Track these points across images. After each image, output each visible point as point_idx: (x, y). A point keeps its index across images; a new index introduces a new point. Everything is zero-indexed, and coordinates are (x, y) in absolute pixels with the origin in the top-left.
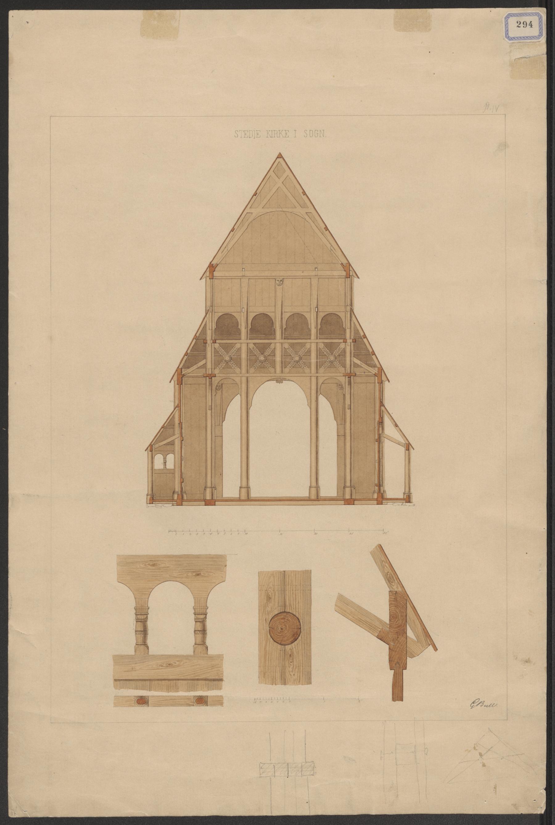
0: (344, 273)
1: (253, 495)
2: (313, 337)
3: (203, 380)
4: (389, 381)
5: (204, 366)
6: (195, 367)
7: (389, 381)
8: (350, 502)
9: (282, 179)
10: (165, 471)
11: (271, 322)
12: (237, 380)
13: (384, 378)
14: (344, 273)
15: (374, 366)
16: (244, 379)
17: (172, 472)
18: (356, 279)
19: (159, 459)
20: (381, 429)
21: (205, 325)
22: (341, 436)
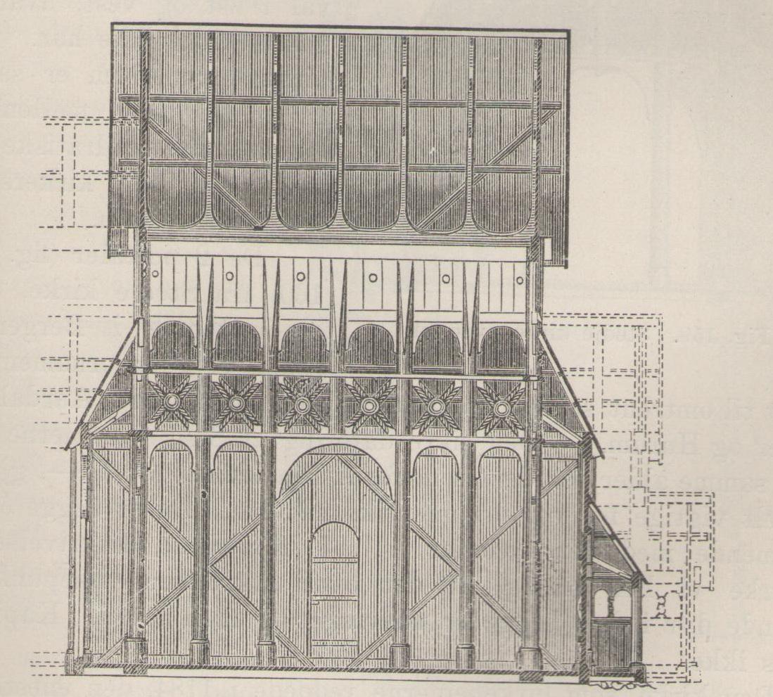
13: (595, 452)
18: (599, 460)
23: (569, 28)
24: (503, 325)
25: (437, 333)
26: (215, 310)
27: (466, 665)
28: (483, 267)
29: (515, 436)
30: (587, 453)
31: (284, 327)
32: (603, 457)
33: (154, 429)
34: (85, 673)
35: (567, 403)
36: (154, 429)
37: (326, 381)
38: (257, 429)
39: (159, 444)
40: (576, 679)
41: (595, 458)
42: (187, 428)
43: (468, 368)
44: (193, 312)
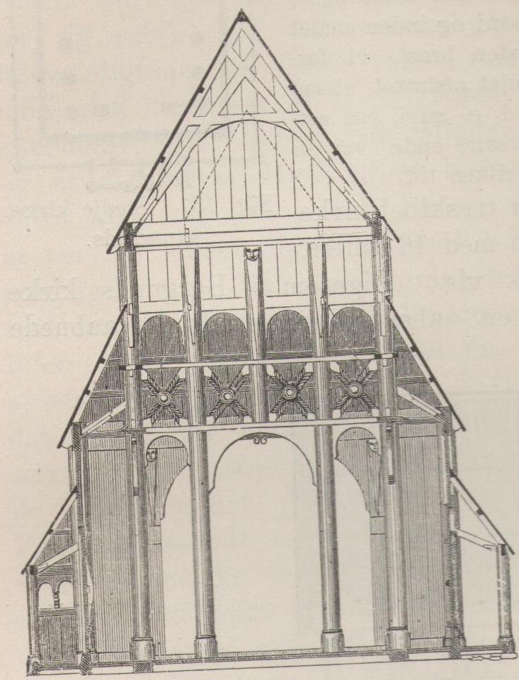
0: (369, 231)
1: (153, 220)
2: (319, 350)
3: (120, 443)
4: (398, 241)
5: (122, 416)
6: (107, 417)
7: (398, 241)
8: (400, 657)
9: (249, 62)
10: (58, 611)
11: (244, 332)
12: (184, 438)
13: (456, 425)
14: (369, 231)
15: (434, 401)
16: (196, 438)
17: (72, 613)
18: (459, 434)
19: (46, 592)
20: (452, 517)
21: (120, 339)
22: (380, 536)
23: (239, 10)
24: (352, 306)
25: (290, 319)
26: (203, 303)
27: (402, 642)
28: (203, 254)
29: (177, 425)
30: (448, 431)
31: (269, 315)
32: (463, 429)
33: (150, 426)
34: (410, 658)
35: (424, 381)
36: (150, 426)
37: (309, 368)
38: (183, 422)
39: (341, 435)
40: (446, 655)
41: (454, 432)
42: (306, 417)
43: (319, 350)
44: (370, 298)
